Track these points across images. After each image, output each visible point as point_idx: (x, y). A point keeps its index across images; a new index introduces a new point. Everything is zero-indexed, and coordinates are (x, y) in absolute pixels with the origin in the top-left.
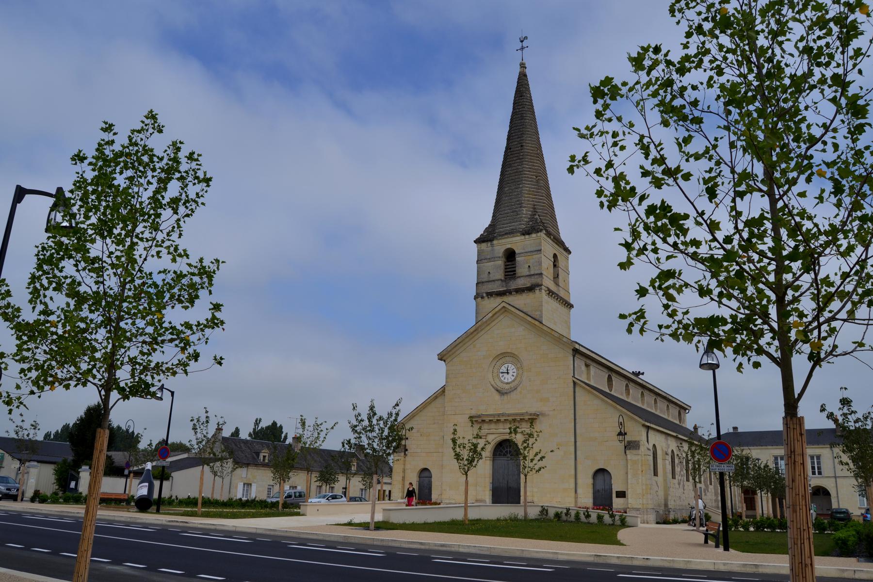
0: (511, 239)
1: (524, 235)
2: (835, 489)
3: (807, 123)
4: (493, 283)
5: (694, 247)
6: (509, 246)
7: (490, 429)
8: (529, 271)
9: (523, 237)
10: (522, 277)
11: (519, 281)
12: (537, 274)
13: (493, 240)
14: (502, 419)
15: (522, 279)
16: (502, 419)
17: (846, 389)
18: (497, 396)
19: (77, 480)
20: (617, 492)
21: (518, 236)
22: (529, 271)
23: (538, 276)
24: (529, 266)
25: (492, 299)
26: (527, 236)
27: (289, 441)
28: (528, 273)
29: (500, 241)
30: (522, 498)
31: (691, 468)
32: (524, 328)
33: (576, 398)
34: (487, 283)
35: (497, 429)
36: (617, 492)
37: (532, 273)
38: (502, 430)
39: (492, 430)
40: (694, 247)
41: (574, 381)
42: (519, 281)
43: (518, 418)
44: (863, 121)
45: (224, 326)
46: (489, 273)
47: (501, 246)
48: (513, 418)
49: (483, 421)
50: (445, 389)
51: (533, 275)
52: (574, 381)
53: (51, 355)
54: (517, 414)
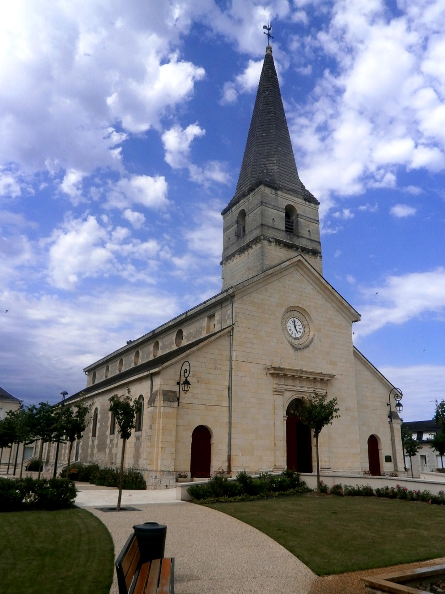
0: (293, 198)
1: (305, 200)
2: (180, 391)
4: (278, 231)
6: (292, 203)
7: (287, 385)
9: (304, 202)
13: (278, 190)
14: (304, 376)
15: (304, 239)
16: (304, 376)
18: (291, 351)
20: (386, 456)
21: (300, 199)
25: (278, 247)
26: (307, 203)
27: (300, 483)
28: (308, 237)
29: (284, 195)
30: (314, 464)
32: (313, 287)
34: (273, 230)
35: (295, 386)
36: (386, 456)
38: (299, 388)
39: (289, 387)
41: (354, 350)
43: (319, 378)
46: (273, 219)
47: (236, 211)
48: (314, 377)
49: (285, 375)
50: (233, 329)
51: (314, 240)
52: (354, 350)
53: (42, 405)
54: (312, 373)
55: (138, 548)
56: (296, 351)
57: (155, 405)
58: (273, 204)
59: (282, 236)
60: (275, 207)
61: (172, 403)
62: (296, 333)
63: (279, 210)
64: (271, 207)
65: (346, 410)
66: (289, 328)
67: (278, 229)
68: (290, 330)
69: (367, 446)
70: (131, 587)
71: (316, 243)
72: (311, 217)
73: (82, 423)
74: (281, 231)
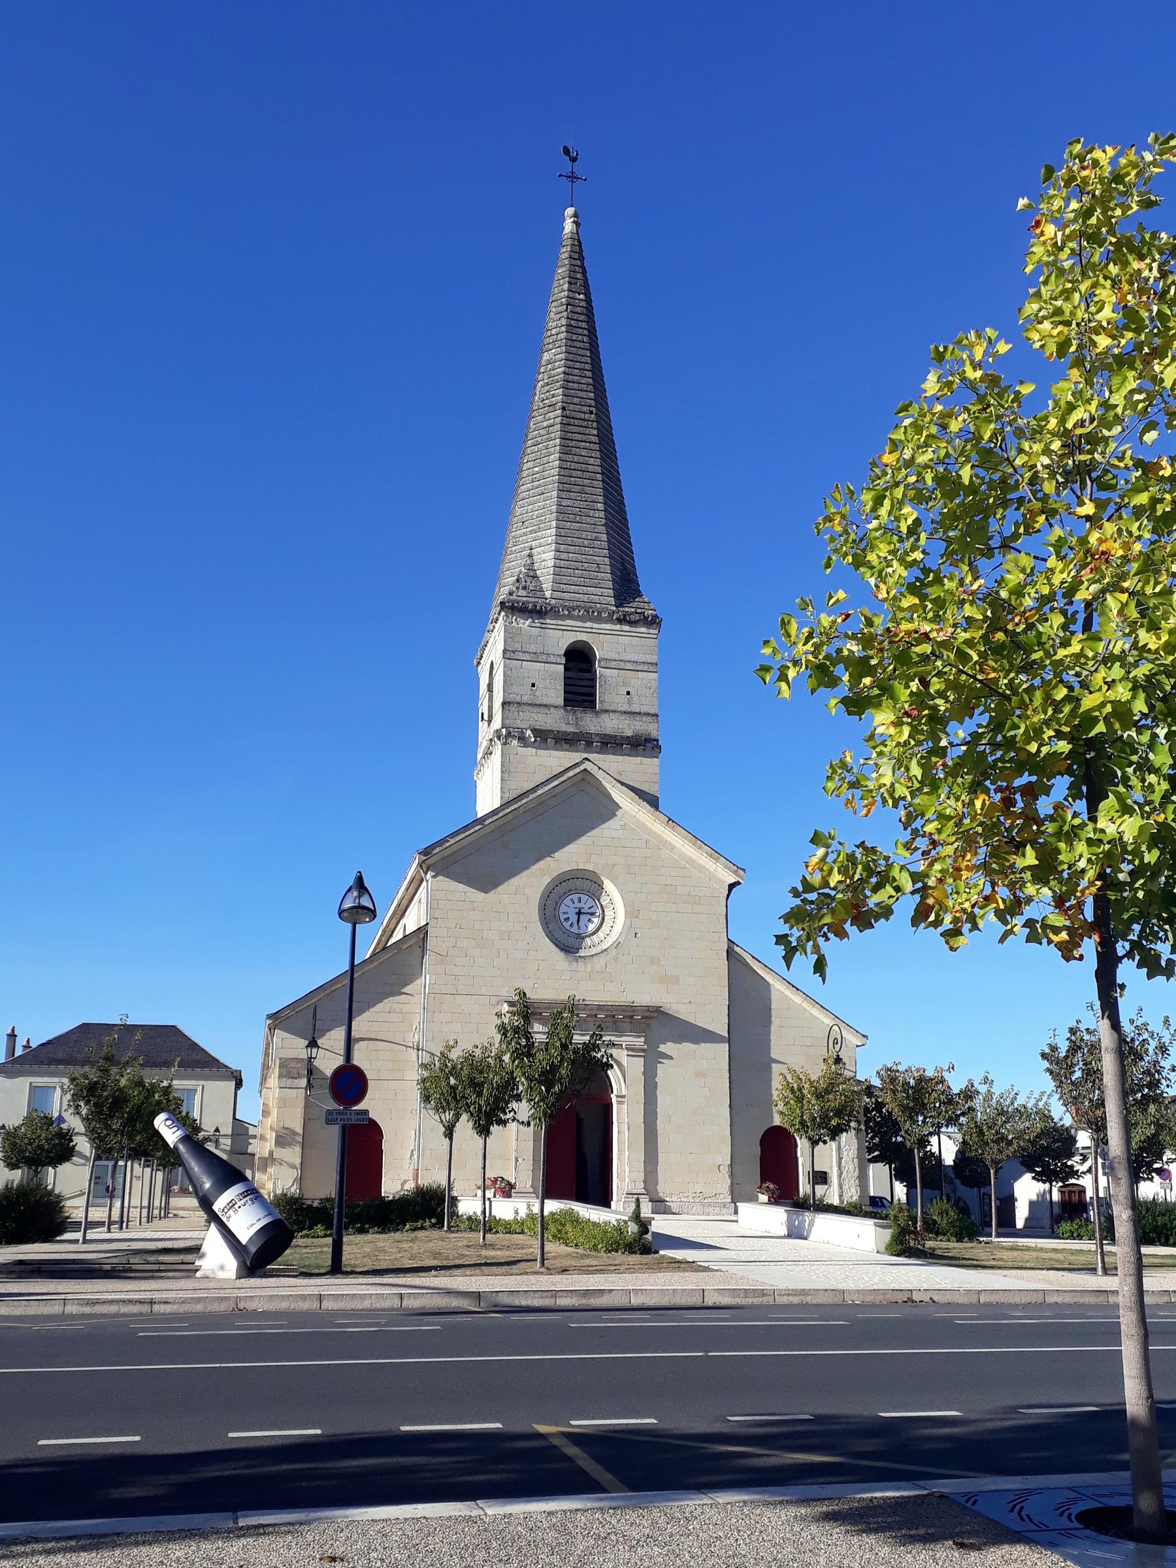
3: (940, 929)
5: (1075, 1169)
8: (630, 703)
10: (614, 711)
11: (607, 720)
12: (647, 714)
17: (566, 151)
19: (1085, 461)
22: (630, 703)
23: (649, 719)
24: (628, 693)
28: (625, 708)
31: (472, 1457)
33: (354, 994)
34: (530, 709)
37: (636, 708)
40: (1075, 1169)
42: (607, 720)
44: (1128, 1322)
45: (1074, 1024)
46: (533, 685)
55: (58, 1238)
56: (575, 964)
57: (267, 1086)
58: (532, 648)
59: (556, 720)
60: (536, 658)
61: (296, 1081)
62: (575, 923)
63: (549, 660)
64: (527, 657)
65: (696, 1075)
66: (563, 917)
67: (545, 706)
68: (567, 919)
69: (757, 1150)
70: (405, 1470)
71: (645, 718)
72: (636, 659)
73: (646, 1231)
74: (552, 710)
